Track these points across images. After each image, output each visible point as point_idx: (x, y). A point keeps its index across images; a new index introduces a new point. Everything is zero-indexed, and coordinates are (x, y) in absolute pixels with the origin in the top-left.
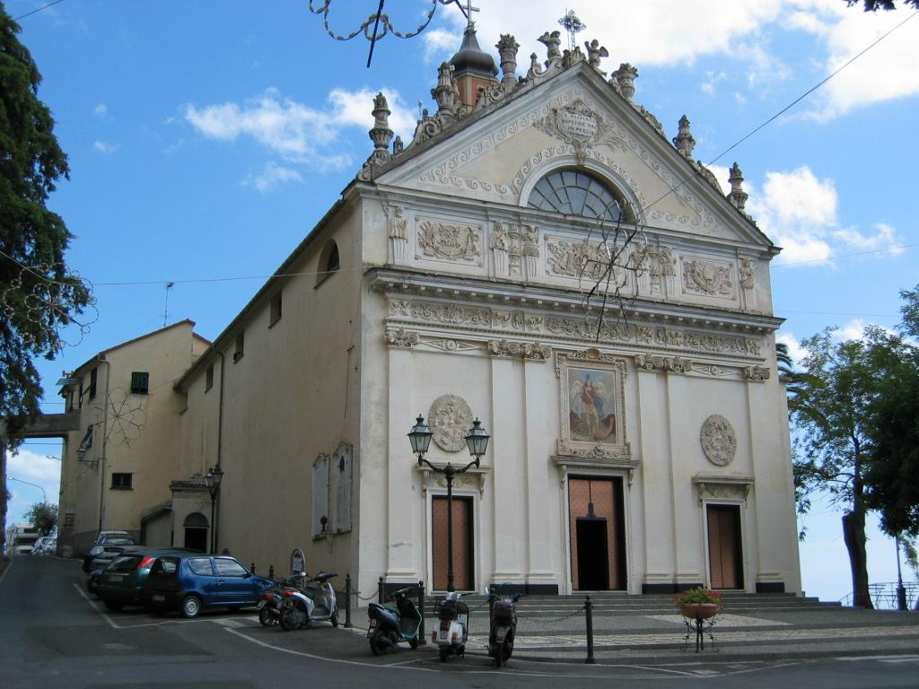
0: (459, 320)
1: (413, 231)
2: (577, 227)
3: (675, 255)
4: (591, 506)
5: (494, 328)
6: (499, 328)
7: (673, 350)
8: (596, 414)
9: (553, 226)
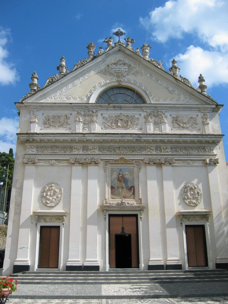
2: (116, 108)
4: (123, 228)
5: (74, 153)
6: (76, 153)
7: (165, 155)
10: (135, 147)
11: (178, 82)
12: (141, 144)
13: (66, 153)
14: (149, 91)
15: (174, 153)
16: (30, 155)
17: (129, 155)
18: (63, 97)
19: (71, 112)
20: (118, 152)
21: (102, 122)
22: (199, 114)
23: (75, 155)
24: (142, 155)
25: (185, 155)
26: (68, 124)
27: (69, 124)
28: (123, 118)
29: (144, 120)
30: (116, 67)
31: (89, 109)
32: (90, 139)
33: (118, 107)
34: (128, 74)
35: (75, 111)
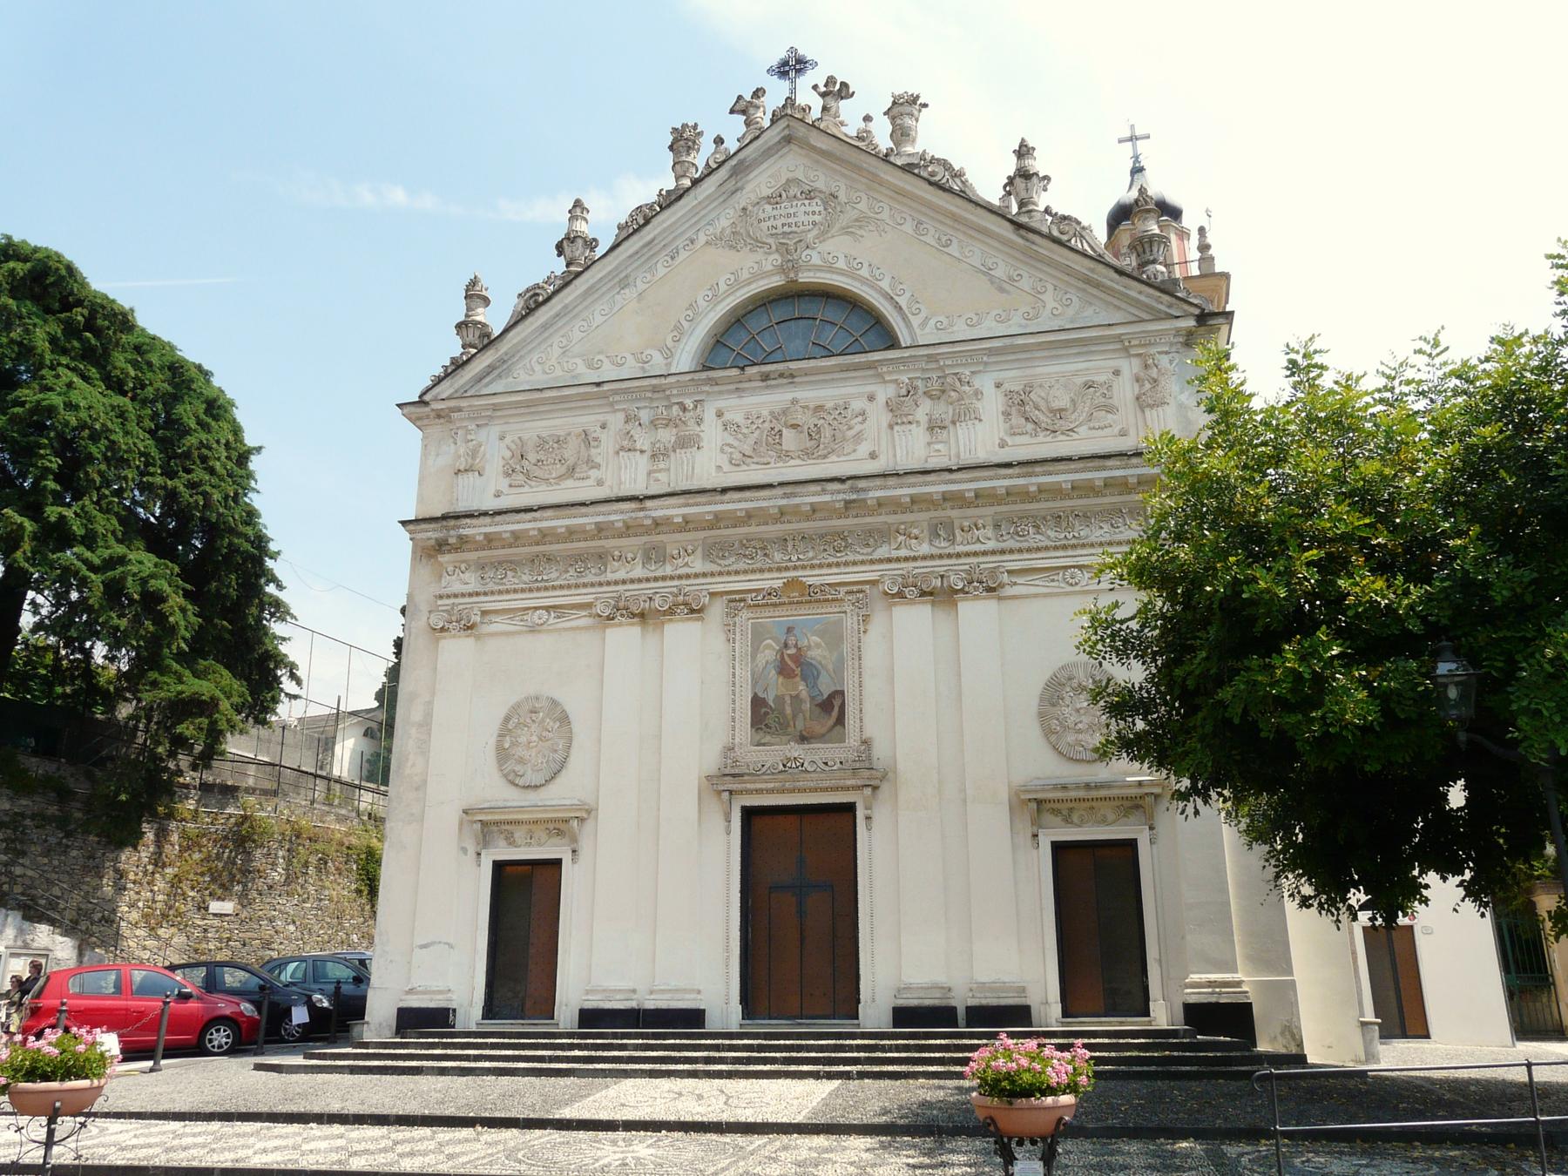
3: (985, 382)
5: (610, 576)
7: (967, 555)
8: (804, 695)
12: (868, 520)
16: (456, 596)
17: (821, 566)
19: (601, 418)
20: (778, 556)
21: (719, 444)
23: (616, 583)
24: (872, 562)
25: (1056, 548)
27: (598, 466)
28: (800, 418)
29: (886, 418)
33: (781, 375)
34: (823, 236)
35: (616, 411)
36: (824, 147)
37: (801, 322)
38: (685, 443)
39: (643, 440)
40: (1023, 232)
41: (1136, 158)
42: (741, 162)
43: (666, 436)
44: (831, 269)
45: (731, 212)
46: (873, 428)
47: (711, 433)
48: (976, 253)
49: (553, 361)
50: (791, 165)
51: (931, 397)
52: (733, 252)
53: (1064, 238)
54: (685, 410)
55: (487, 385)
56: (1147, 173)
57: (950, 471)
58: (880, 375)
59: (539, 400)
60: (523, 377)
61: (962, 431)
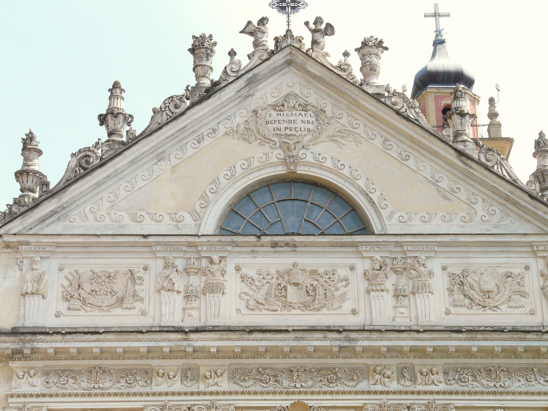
0: (108, 384)
1: (55, 282)
2: (280, 249)
3: (435, 265)
5: (155, 389)
6: (164, 388)
7: (426, 393)
9: (247, 253)
10: (337, 370)
11: (466, 164)
12: (353, 361)
13: (132, 390)
14: (378, 193)
15: (455, 387)
16: (25, 396)
17: (318, 393)
18: (121, 213)
19: (144, 262)
20: (286, 383)
21: (238, 292)
22: (532, 262)
23: (160, 394)
24: (357, 393)
25: (489, 393)
26: (135, 298)
27: (141, 300)
28: (300, 278)
29: (363, 285)
30: (279, 118)
31: (198, 252)
32: (204, 347)
33: (287, 244)
34: (315, 140)
35: (156, 258)
36: (318, 73)
37: (297, 205)
38: (214, 288)
39: (180, 283)
40: (464, 159)
41: (438, 33)
42: (255, 76)
43: (197, 282)
44: (321, 167)
45: (245, 112)
46: (353, 292)
47: (232, 283)
48: (427, 168)
49: (103, 212)
50: (288, 83)
51: (396, 272)
52: (246, 143)
53: (489, 164)
54: (212, 262)
55: (48, 226)
56: (447, 44)
57: (418, 331)
58: (360, 252)
59: (94, 242)
60: (78, 222)
61: (420, 300)
